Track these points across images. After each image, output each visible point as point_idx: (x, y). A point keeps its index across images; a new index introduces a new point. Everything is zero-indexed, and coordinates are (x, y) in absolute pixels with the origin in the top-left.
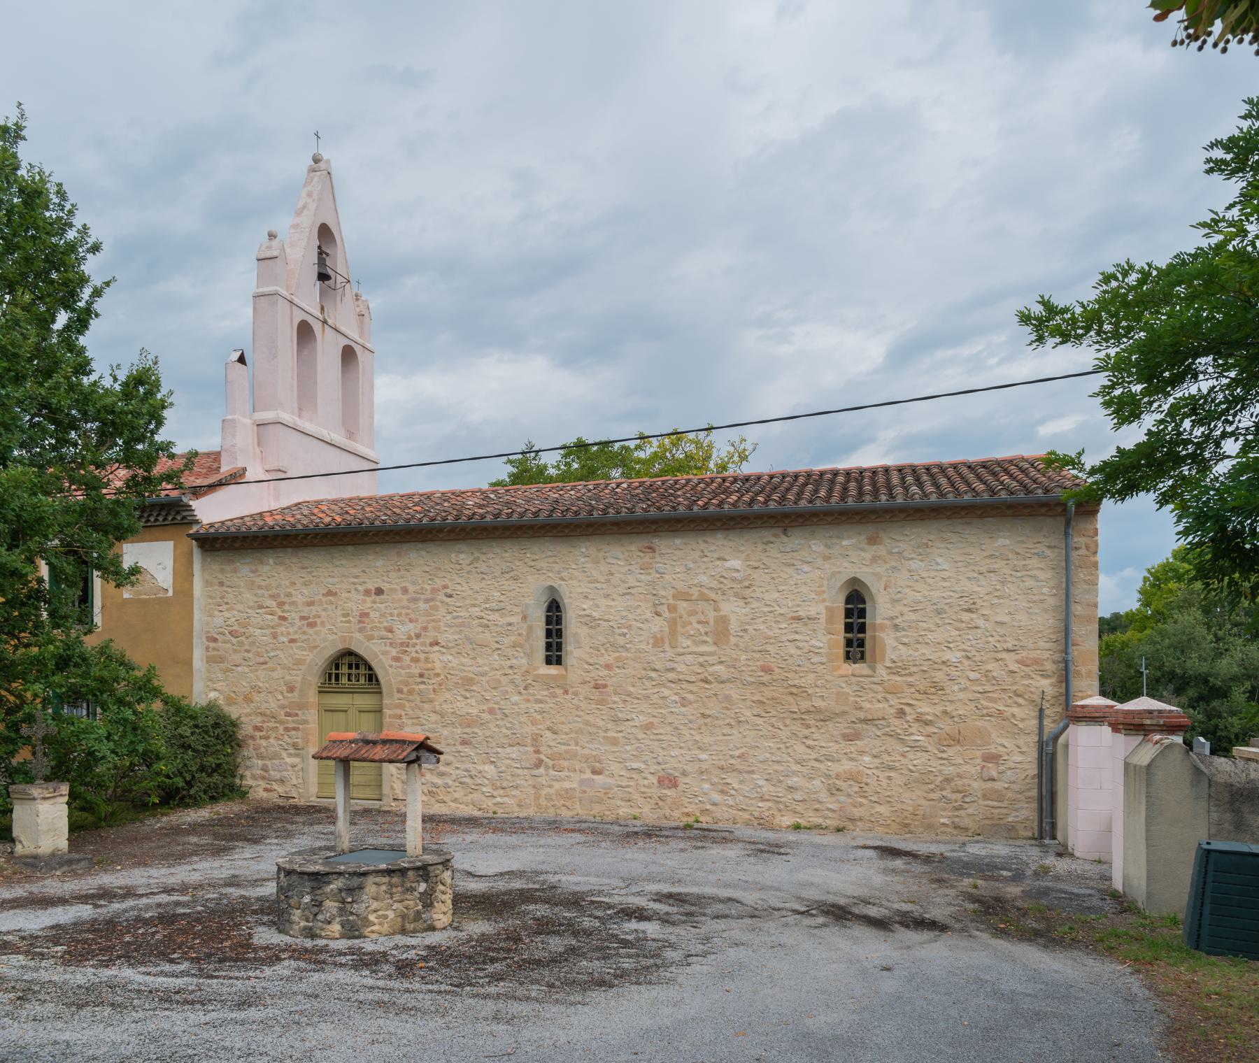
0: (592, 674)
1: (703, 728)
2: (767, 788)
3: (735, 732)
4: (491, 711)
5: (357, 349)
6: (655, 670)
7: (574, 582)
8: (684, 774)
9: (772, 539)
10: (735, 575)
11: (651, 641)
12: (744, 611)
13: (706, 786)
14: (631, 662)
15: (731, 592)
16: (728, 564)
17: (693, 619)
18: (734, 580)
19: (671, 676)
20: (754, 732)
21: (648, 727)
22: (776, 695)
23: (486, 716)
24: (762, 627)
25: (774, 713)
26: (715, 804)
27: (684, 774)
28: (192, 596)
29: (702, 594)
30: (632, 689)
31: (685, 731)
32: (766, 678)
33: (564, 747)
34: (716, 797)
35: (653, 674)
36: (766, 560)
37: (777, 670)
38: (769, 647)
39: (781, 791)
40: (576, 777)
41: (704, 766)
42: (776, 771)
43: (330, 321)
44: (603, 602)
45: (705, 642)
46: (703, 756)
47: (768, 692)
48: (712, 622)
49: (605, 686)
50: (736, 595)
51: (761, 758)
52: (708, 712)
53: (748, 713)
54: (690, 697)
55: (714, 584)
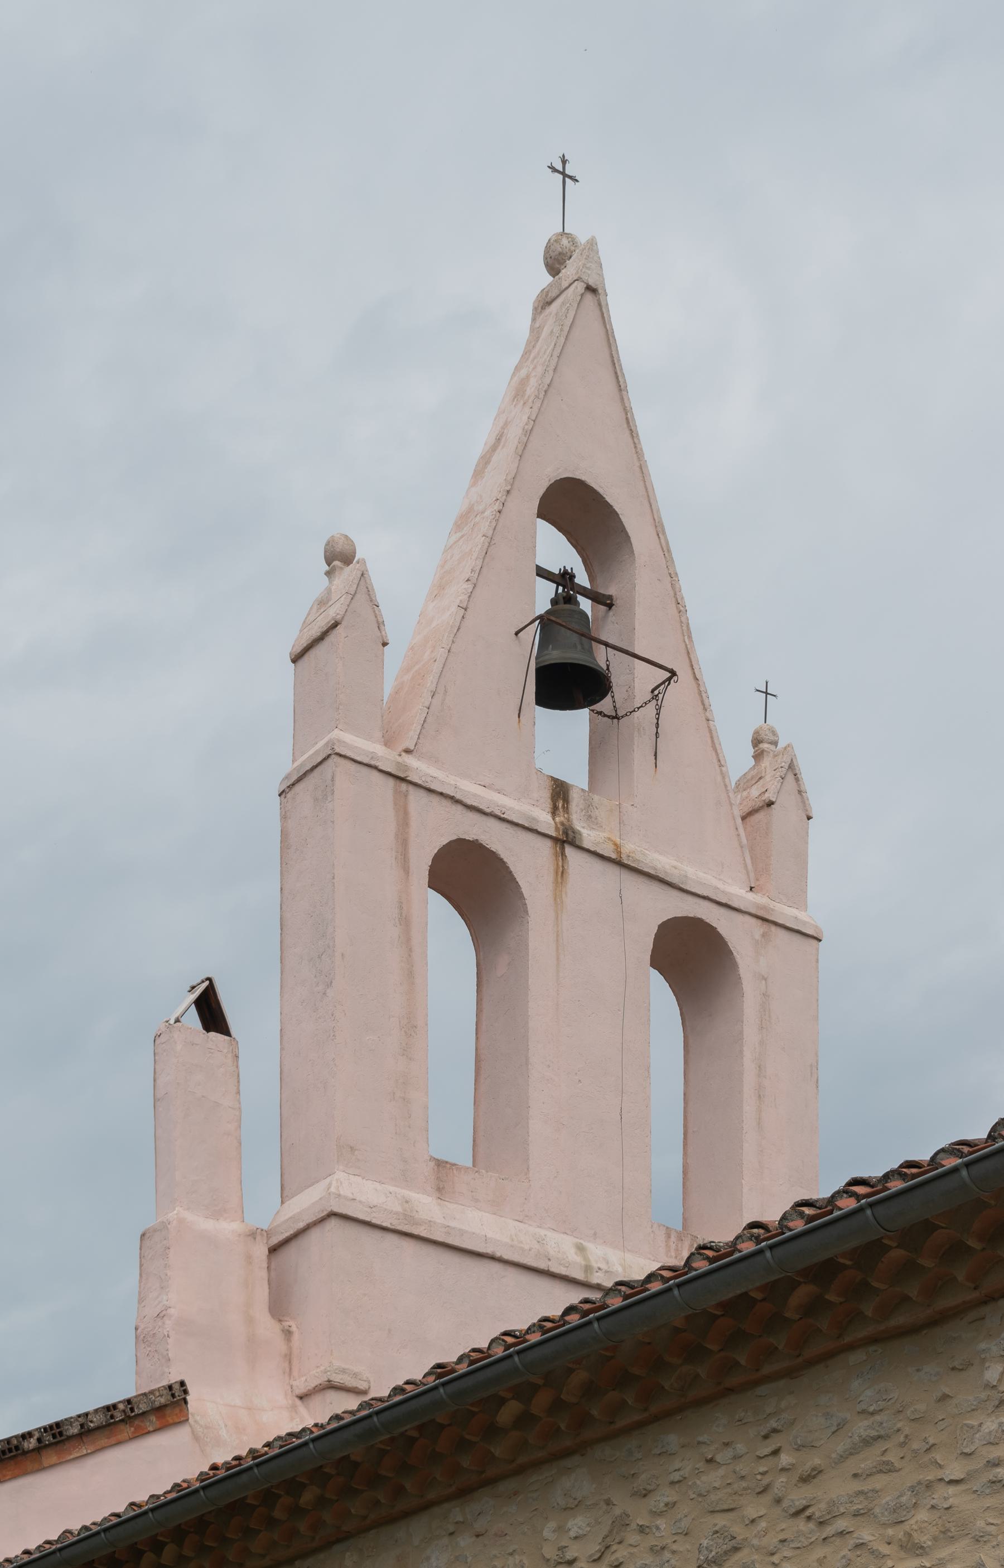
5: (734, 931)
43: (589, 837)
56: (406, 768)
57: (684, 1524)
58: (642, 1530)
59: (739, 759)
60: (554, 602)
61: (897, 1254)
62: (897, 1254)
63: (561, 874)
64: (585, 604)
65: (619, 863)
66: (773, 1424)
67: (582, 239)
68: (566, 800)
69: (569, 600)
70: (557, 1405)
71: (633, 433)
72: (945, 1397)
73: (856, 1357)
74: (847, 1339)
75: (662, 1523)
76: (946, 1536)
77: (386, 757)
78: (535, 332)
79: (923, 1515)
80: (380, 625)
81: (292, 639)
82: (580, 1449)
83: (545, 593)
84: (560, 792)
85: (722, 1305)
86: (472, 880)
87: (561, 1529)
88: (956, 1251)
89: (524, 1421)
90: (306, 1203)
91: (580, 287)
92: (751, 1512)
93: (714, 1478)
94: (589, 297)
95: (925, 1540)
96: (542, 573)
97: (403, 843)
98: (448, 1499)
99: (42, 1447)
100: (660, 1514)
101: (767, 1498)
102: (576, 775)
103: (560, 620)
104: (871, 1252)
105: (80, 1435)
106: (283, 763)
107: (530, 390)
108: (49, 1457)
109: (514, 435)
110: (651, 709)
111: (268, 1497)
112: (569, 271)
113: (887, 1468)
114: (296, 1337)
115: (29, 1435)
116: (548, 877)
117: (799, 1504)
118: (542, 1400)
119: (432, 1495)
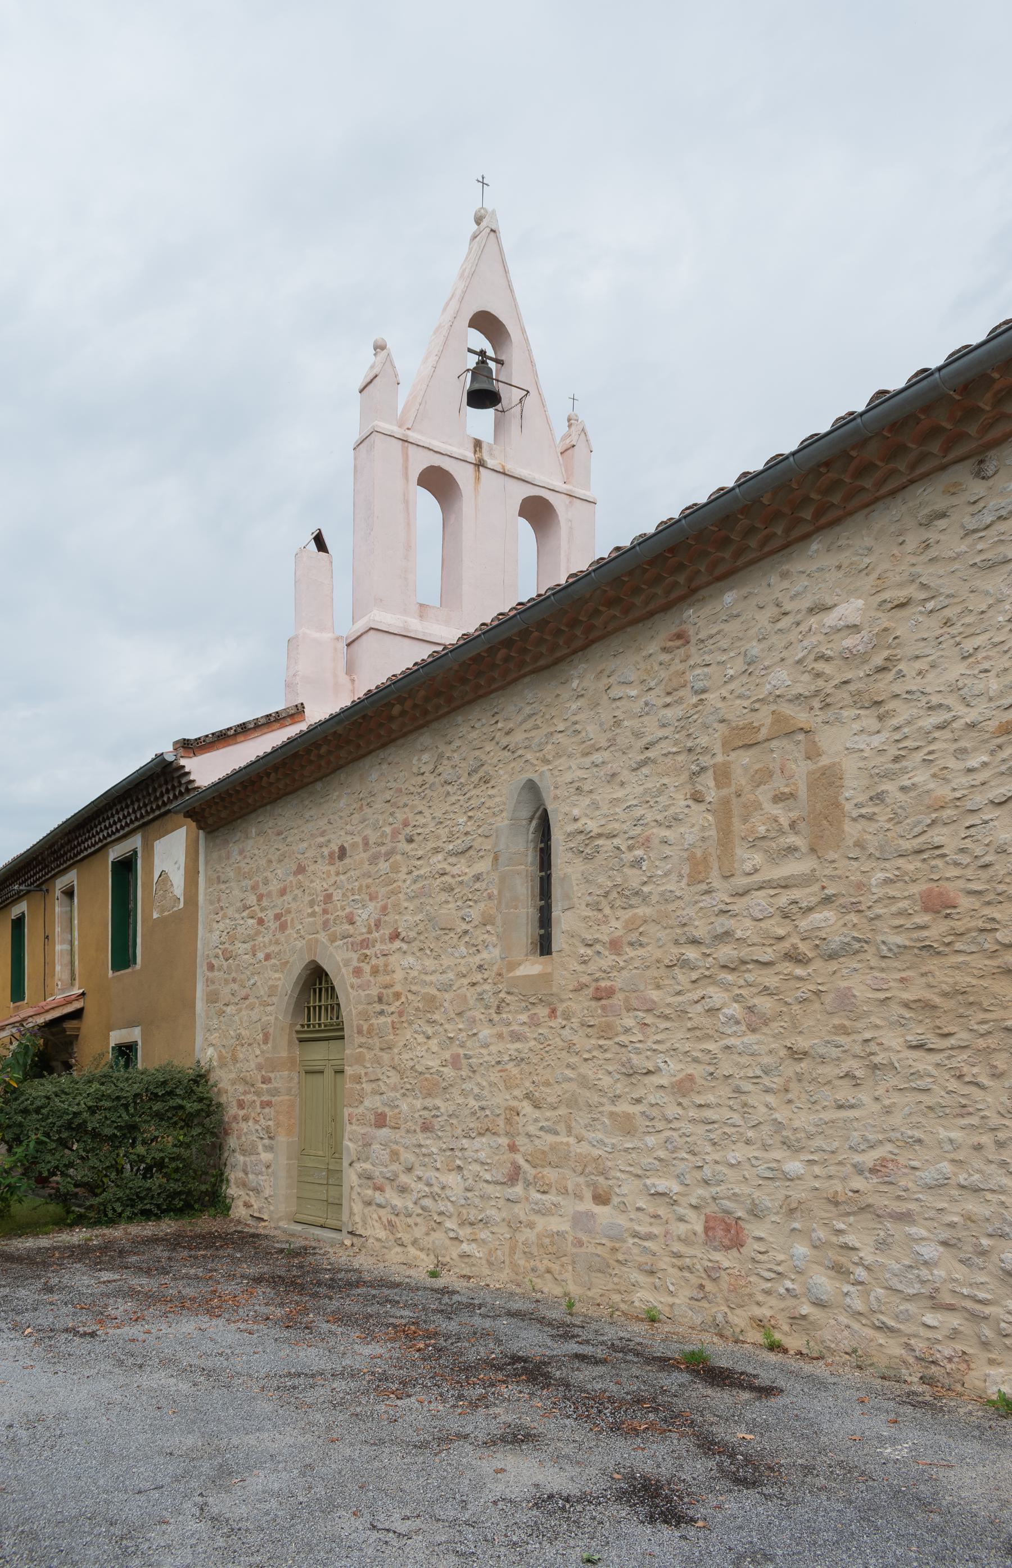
0: (592, 967)
1: (794, 1086)
2: (947, 1270)
3: (865, 1097)
4: (455, 1062)
5: (557, 502)
6: (695, 942)
7: (562, 762)
8: (756, 1213)
9: (941, 504)
10: (850, 641)
11: (686, 870)
12: (876, 741)
13: (801, 1249)
14: (652, 929)
15: (843, 695)
16: (831, 619)
17: (764, 795)
18: (849, 657)
19: (726, 952)
20: (912, 1098)
21: (683, 1087)
22: (964, 980)
23: (448, 1072)
24: (921, 777)
25: (963, 1036)
26: (819, 1304)
27: (756, 1213)
28: (197, 905)
29: (778, 718)
30: (654, 995)
31: (757, 1099)
32: (938, 930)
33: (550, 1138)
34: (824, 1283)
35: (692, 953)
36: (928, 574)
37: (965, 903)
38: (939, 836)
39: (984, 1282)
40: (571, 1206)
41: (798, 1194)
42: (969, 1218)
43: (490, 462)
44: (607, 793)
45: (792, 850)
46: (794, 1166)
47: (942, 973)
48: (803, 792)
49: (610, 993)
50: (858, 700)
51: (928, 1175)
52: (802, 1043)
53: (893, 1039)
54: (765, 1004)
55: (805, 685)
56: (407, 436)
57: (464, 755)
58: (448, 758)
59: (560, 428)
60: (477, 363)
61: (536, 634)
62: (536, 634)
63: (478, 479)
64: (492, 365)
65: (504, 474)
66: (495, 710)
67: (490, 210)
68: (481, 447)
69: (483, 362)
70: (415, 706)
71: (512, 291)
72: (558, 695)
73: (526, 680)
74: (522, 672)
75: (455, 755)
76: (558, 756)
77: (398, 432)
78: (470, 249)
79: (549, 747)
80: (396, 376)
81: (360, 383)
82: (426, 725)
83: (472, 361)
84: (478, 444)
85: (471, 659)
86: (438, 482)
87: (419, 760)
88: (559, 632)
89: (403, 713)
90: (361, 625)
91: (488, 230)
92: (488, 749)
93: (474, 734)
94: (492, 234)
95: (550, 757)
96: (470, 350)
97: (406, 468)
98: (378, 748)
99: (236, 734)
100: (455, 751)
101: (494, 742)
102: (487, 436)
103: (481, 370)
104: (525, 633)
105: (254, 728)
106: (356, 437)
107: (466, 274)
108: (240, 738)
109: (459, 293)
110: (519, 407)
111: (308, 751)
112: (483, 224)
113: (537, 727)
114: (356, 682)
115: (231, 728)
116: (472, 481)
117: (505, 744)
118: (408, 704)
119: (371, 748)
